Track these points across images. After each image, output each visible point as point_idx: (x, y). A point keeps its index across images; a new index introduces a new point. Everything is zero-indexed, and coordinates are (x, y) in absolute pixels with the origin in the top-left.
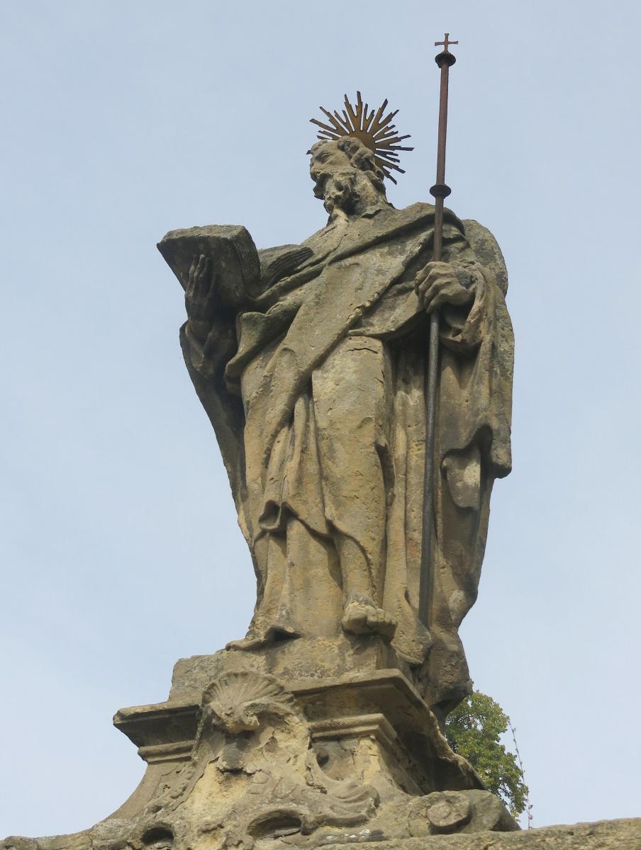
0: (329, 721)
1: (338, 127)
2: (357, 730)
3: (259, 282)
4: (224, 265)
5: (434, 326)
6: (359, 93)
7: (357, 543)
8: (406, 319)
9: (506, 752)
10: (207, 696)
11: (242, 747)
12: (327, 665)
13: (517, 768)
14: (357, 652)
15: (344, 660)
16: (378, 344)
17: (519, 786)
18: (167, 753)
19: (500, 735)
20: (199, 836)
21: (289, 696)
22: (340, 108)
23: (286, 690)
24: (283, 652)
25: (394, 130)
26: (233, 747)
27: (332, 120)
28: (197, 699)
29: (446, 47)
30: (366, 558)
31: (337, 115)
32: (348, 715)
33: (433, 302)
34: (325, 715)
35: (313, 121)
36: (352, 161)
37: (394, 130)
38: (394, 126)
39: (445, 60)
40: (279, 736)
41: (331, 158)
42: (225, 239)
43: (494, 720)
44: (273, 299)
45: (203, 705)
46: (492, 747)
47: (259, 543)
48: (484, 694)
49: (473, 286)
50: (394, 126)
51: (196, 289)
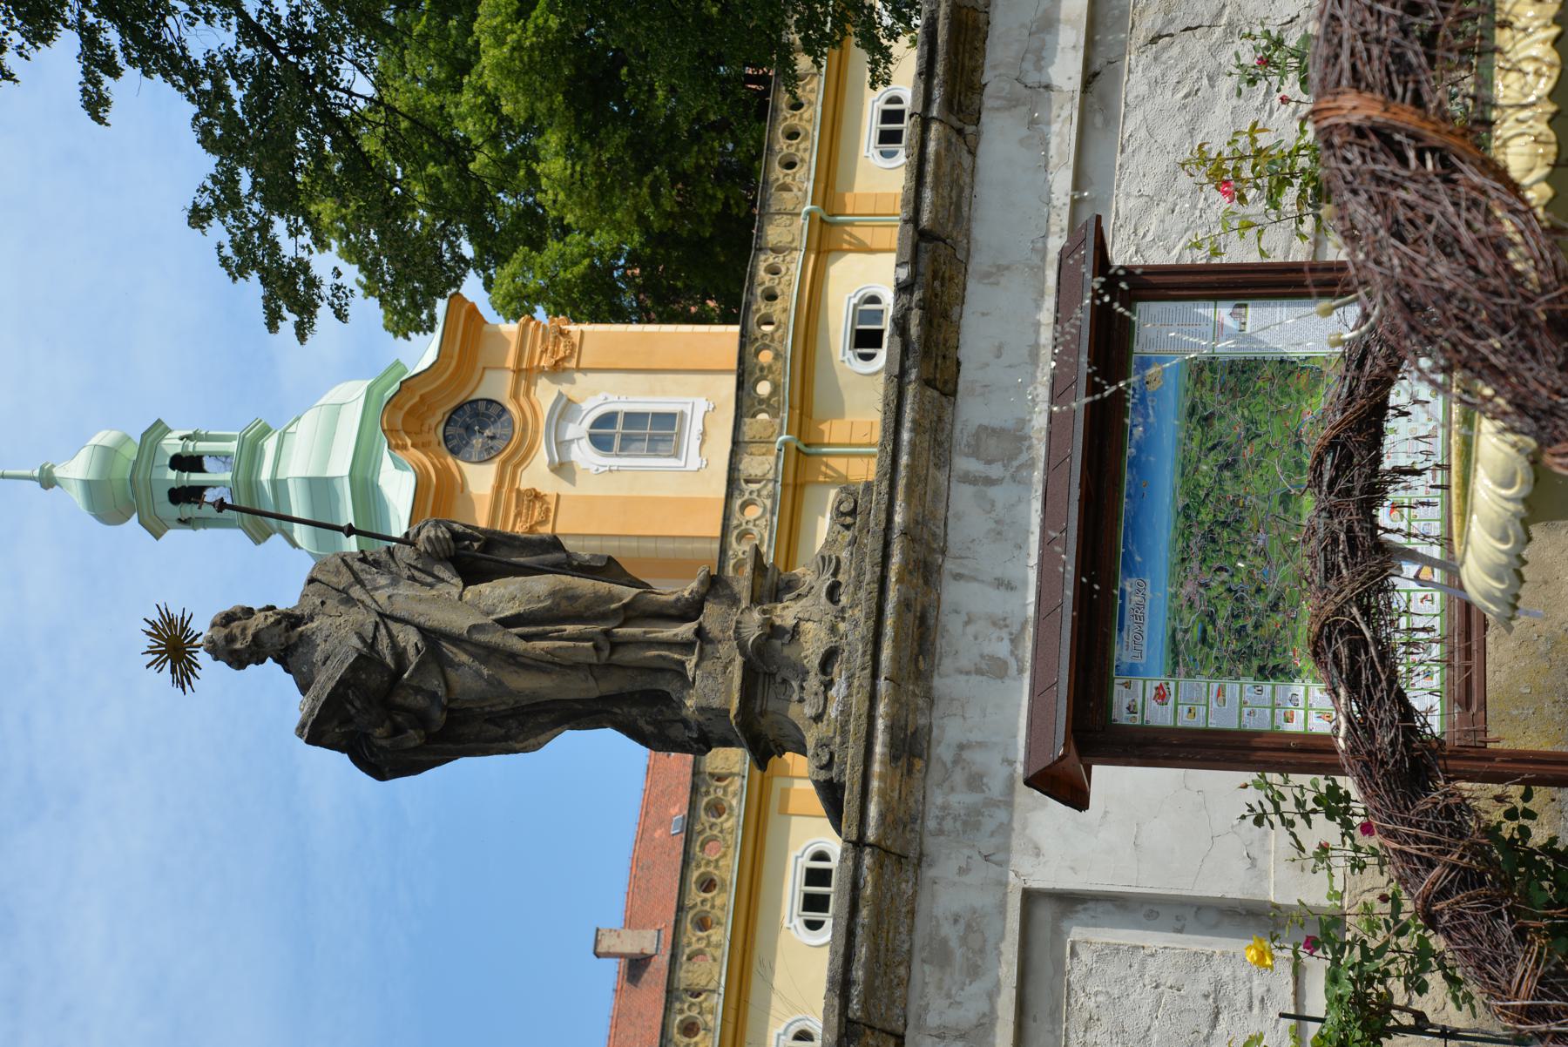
27: (154, 653)
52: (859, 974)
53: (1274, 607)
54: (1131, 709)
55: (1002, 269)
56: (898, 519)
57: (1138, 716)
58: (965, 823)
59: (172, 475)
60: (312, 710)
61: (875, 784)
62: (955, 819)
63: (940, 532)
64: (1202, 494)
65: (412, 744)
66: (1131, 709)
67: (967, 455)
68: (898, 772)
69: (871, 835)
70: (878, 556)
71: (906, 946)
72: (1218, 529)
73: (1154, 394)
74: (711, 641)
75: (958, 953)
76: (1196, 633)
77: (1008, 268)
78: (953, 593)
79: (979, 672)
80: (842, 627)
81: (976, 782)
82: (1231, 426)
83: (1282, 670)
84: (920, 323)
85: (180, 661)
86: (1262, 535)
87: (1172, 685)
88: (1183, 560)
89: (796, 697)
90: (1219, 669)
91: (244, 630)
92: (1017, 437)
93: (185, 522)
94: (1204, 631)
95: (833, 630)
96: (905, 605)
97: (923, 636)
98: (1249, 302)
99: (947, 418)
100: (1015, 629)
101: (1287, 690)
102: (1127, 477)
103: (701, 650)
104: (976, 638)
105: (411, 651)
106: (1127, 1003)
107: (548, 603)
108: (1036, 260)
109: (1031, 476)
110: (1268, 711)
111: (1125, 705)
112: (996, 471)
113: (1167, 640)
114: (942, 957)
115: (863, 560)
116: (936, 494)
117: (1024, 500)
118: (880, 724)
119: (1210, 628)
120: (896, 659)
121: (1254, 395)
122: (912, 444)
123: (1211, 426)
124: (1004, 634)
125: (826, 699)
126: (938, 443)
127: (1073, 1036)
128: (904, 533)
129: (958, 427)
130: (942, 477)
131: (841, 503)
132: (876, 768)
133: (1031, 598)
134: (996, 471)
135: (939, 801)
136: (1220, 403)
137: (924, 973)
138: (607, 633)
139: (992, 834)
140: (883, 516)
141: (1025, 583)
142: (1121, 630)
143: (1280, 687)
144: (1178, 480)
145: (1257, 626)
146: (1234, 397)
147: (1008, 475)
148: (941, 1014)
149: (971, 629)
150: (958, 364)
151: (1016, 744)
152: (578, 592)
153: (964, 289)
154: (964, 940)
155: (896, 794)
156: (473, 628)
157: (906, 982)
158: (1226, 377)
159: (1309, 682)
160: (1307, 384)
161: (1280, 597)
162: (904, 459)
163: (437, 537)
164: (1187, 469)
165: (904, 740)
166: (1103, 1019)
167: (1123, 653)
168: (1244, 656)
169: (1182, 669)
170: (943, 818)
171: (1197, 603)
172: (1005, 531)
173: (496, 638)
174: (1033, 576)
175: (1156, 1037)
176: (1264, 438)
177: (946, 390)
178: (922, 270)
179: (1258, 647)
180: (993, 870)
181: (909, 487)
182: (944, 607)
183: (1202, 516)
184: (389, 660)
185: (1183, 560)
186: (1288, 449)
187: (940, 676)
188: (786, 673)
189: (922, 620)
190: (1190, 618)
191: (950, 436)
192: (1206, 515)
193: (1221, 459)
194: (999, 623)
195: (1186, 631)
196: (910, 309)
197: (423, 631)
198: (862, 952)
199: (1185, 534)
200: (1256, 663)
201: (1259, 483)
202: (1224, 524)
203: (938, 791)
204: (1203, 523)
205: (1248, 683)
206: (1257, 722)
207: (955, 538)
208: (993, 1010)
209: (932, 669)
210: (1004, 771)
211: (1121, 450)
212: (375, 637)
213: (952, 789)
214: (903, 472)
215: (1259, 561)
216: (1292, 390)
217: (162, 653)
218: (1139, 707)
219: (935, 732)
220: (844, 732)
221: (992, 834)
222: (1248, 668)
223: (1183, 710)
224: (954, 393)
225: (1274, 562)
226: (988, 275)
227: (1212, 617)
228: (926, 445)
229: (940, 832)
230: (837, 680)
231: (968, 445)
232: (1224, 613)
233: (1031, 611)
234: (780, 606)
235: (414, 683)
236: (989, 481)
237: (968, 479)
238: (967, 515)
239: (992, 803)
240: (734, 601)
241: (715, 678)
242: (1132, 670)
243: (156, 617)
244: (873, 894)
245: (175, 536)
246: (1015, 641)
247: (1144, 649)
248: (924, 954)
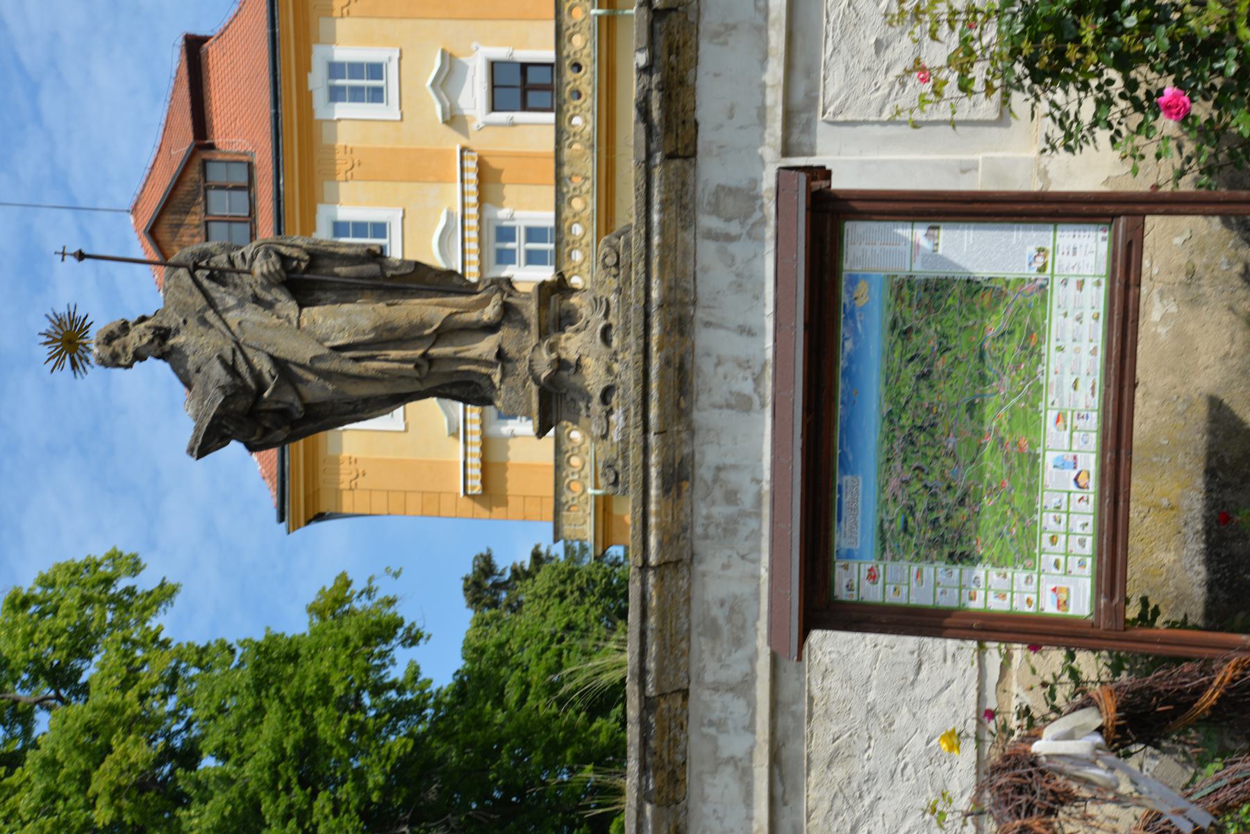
27: (53, 357)
52: (651, 665)
53: (961, 502)
54: (849, 587)
55: (731, 28)
56: (655, 294)
57: (855, 592)
58: (725, 530)
60: (197, 438)
61: (653, 520)
62: (717, 526)
63: (690, 287)
64: (903, 401)
66: (849, 587)
67: (710, 213)
68: (670, 501)
69: (653, 560)
70: (641, 329)
71: (686, 627)
72: (916, 433)
73: (861, 309)
74: (510, 360)
75: (725, 629)
76: (899, 523)
77: (734, 27)
78: (704, 339)
79: (729, 406)
80: (616, 367)
81: (731, 497)
82: (926, 339)
83: (967, 556)
84: (661, 107)
85: (75, 351)
86: (952, 439)
87: (881, 568)
88: (888, 460)
89: (583, 412)
90: (917, 554)
91: (124, 348)
92: (751, 196)
94: (906, 522)
95: (609, 370)
96: (666, 363)
97: (681, 379)
98: (942, 225)
99: (690, 181)
100: (757, 369)
101: (971, 574)
102: (841, 385)
103: (503, 369)
104: (725, 377)
105: (267, 377)
106: (853, 658)
107: (372, 336)
108: (759, 20)
109: (764, 233)
110: (956, 591)
111: (844, 584)
112: (734, 228)
113: (876, 529)
114: (713, 631)
115: (628, 309)
116: (685, 253)
117: (758, 255)
118: (653, 472)
119: (910, 519)
120: (662, 416)
121: (946, 311)
122: (662, 223)
123: (909, 339)
124: (748, 374)
125: (608, 422)
126: (684, 207)
127: (813, 683)
128: (660, 306)
129: (700, 187)
130: (688, 236)
131: (605, 256)
132: (653, 507)
133: (769, 343)
134: (734, 228)
135: (704, 512)
136: (917, 318)
137: (700, 643)
138: (424, 355)
139: (747, 538)
140: (642, 294)
141: (763, 329)
142: (839, 520)
143: (966, 571)
144: (883, 389)
145: (948, 518)
146: (929, 312)
147: (744, 232)
148: (715, 673)
149: (721, 370)
150: (696, 124)
151: (761, 466)
152: (396, 324)
153: (697, 49)
154: (729, 619)
155: (670, 519)
156: (313, 359)
157: (687, 653)
158: (922, 293)
159: (989, 567)
160: (990, 303)
161: (965, 494)
162: (656, 240)
163: (269, 272)
164: (892, 379)
165: (673, 475)
166: (836, 671)
167: (842, 538)
168: (937, 543)
169: (888, 554)
170: (708, 526)
171: (900, 498)
172: (745, 283)
173: (334, 365)
174: (769, 324)
175: (875, 683)
176: (953, 351)
177: (687, 154)
178: (658, 53)
179: (948, 536)
180: (749, 567)
181: (662, 264)
182: (699, 350)
183: (903, 421)
184: (249, 381)
185: (888, 460)
186: (973, 361)
187: (698, 410)
188: (576, 396)
189: (681, 368)
190: (895, 510)
191: (694, 198)
192: (906, 421)
193: (919, 370)
194: (744, 364)
195: (891, 522)
196: (650, 90)
197: (274, 360)
198: (653, 649)
199: (889, 437)
200: (947, 550)
201: (950, 393)
202: (921, 429)
203: (702, 505)
204: (903, 427)
205: (941, 566)
206: (947, 600)
207: (704, 290)
208: (753, 670)
209: (691, 403)
210: (753, 488)
211: (834, 362)
212: (234, 360)
213: (714, 503)
214: (655, 252)
215: (949, 462)
216: (977, 308)
217: (59, 353)
218: (855, 586)
219: (697, 457)
220: (624, 454)
221: (747, 538)
222: (941, 554)
223: (890, 588)
224: (694, 154)
225: (962, 463)
226: (717, 35)
227: (911, 510)
229: (706, 537)
230: (615, 409)
231: (709, 203)
232: (921, 507)
233: (769, 354)
234: (564, 336)
235: (274, 398)
236: (729, 238)
237: (712, 235)
238: (713, 269)
239: (744, 514)
240: (525, 325)
241: (517, 392)
242: (849, 555)
244: (658, 605)
246: (758, 380)
247: (859, 535)
248: (700, 629)
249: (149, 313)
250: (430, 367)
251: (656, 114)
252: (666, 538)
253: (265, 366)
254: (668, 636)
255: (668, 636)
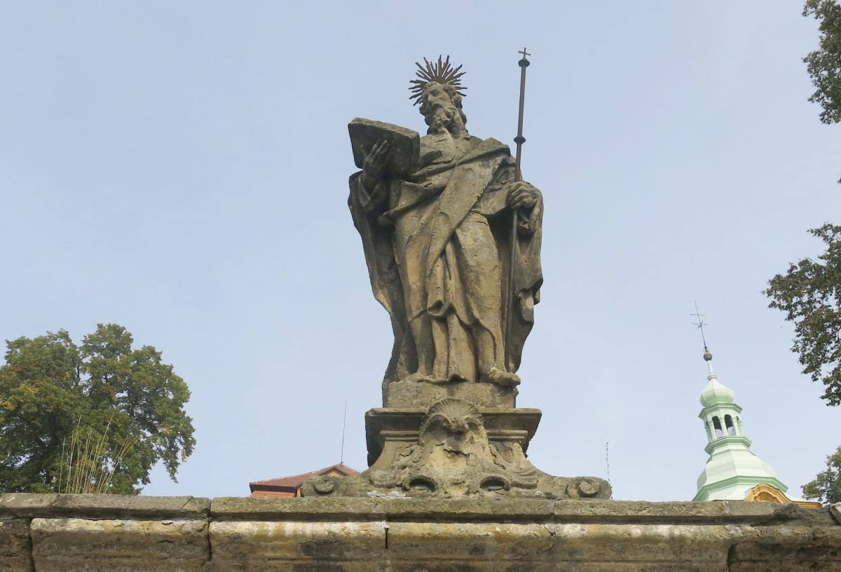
0: (497, 431)
1: (430, 72)
2: (513, 437)
3: (417, 166)
4: (399, 150)
5: (515, 217)
6: (448, 57)
7: (491, 334)
8: (500, 209)
9: (186, 415)
10: (433, 409)
11: (458, 439)
12: (485, 399)
13: (191, 427)
14: (502, 395)
15: (494, 398)
16: (485, 220)
17: (190, 439)
18: (399, 436)
19: (184, 404)
20: (451, 486)
21: (481, 415)
22: (435, 61)
23: (479, 412)
24: (458, 388)
25: (459, 82)
26: (452, 439)
27: (428, 67)
28: (425, 409)
29: (524, 56)
30: (494, 342)
31: (431, 65)
32: (507, 429)
33: (518, 204)
34: (494, 427)
35: (417, 64)
36: (452, 100)
37: (459, 82)
38: (460, 80)
39: (524, 64)
40: (474, 436)
41: (440, 96)
42: (407, 138)
43: (182, 393)
44: (422, 178)
45: (429, 413)
46: (178, 411)
47: (416, 320)
48: (178, 375)
49: (536, 200)
50: (460, 80)
51: (375, 159)
52: (74, 524)
56: (570, 530)
59: (723, 416)
61: (271, 527)
65: (361, 202)
68: (293, 555)
69: (215, 527)
93: (707, 424)
118: (335, 527)
122: (655, 540)
132: (290, 527)
155: (270, 554)
162: (636, 530)
181: (605, 541)
198: (94, 526)
228: (661, 557)
241: (415, 397)
243: (454, 66)
245: (701, 423)
249: (467, 126)
250: (437, 319)
251: (784, 531)
252: (243, 549)
253: (436, 181)
254: (111, 552)
255: (111, 552)
